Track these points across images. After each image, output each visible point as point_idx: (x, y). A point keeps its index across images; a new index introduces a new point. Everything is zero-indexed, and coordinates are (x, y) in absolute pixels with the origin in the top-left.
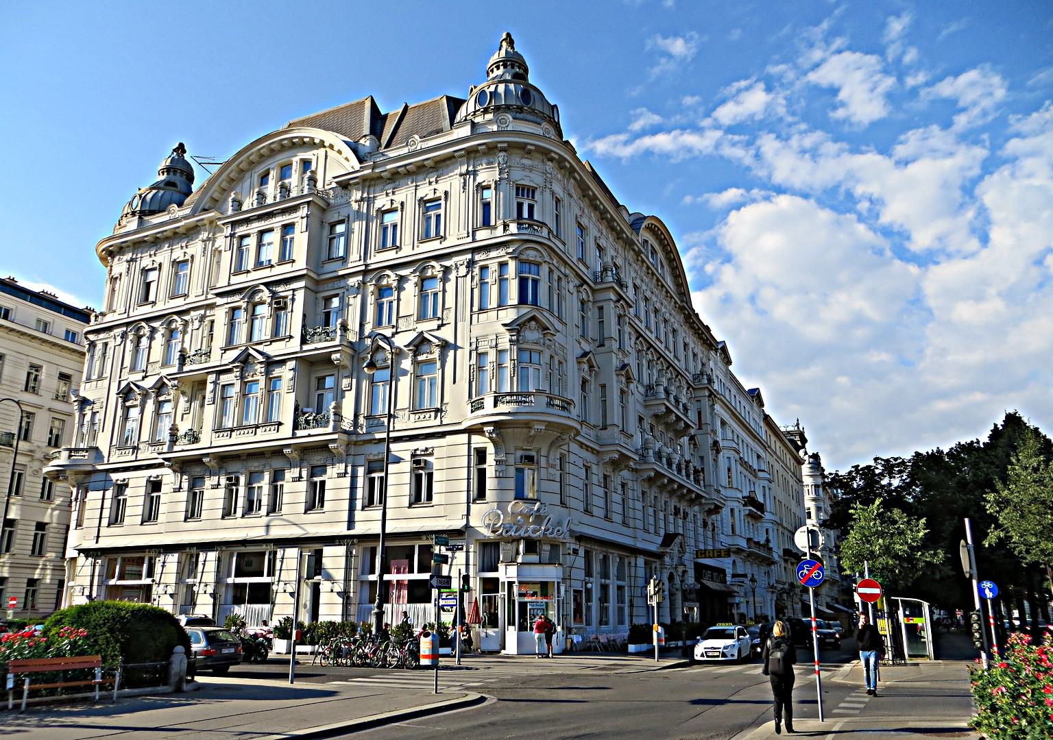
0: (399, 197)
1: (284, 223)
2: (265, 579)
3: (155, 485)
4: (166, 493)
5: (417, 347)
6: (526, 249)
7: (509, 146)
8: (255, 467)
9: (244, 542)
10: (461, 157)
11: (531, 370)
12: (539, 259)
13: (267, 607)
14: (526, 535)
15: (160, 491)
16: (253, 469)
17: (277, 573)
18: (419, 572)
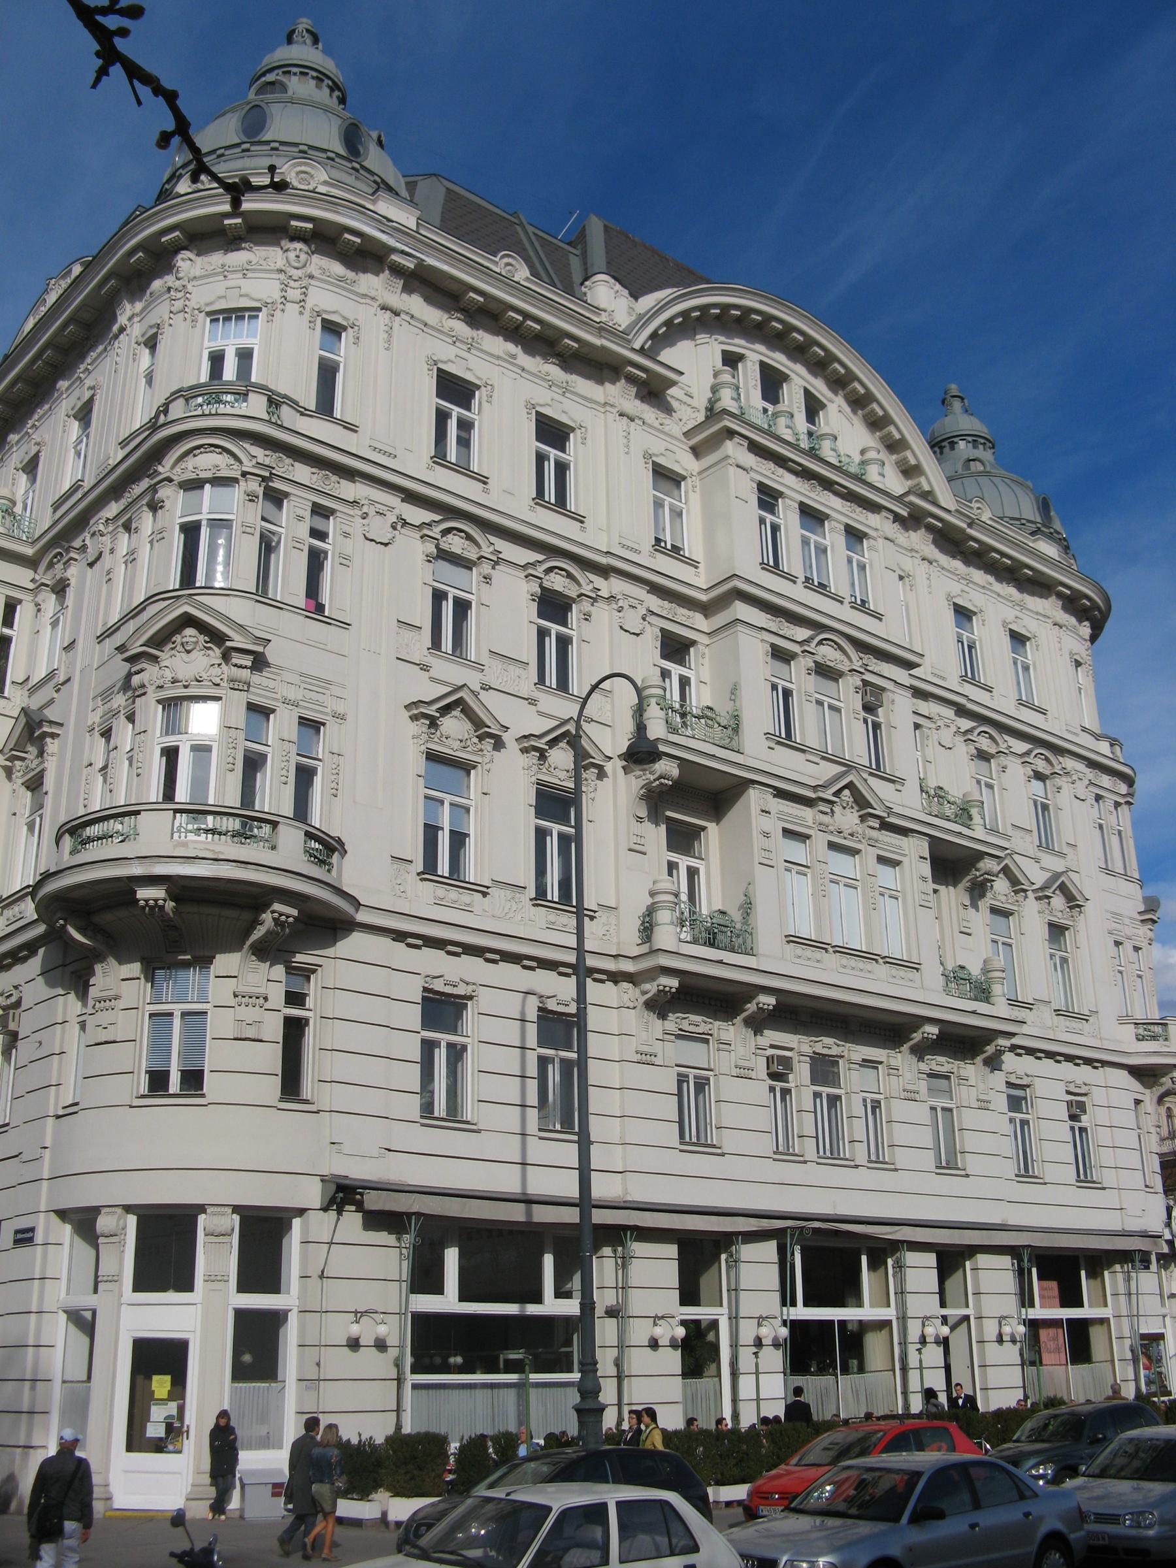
10: (631, 379)
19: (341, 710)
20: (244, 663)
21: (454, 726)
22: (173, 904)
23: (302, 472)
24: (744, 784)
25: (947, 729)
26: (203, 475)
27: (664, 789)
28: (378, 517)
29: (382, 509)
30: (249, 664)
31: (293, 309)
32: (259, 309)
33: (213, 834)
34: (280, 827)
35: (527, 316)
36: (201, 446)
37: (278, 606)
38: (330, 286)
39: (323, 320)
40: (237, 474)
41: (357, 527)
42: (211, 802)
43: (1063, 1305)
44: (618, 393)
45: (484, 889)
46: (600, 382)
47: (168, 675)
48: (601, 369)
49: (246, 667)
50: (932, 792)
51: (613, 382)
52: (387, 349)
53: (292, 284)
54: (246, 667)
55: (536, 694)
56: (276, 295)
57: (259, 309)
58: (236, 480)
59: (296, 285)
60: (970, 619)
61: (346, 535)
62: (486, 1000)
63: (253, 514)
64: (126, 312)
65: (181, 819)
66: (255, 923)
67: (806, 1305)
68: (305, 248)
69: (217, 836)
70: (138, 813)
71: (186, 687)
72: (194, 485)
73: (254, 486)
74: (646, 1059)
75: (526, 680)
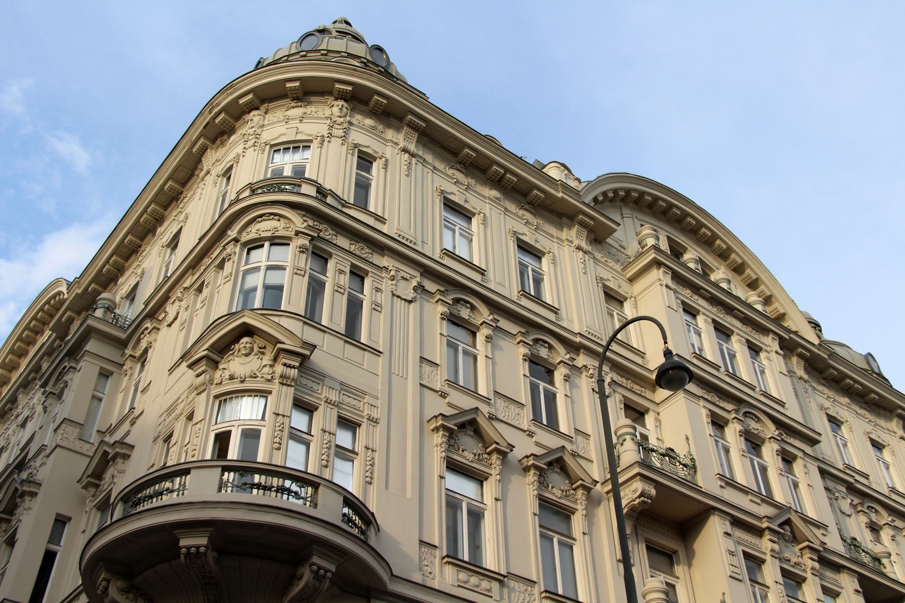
10: (582, 224)
19: (375, 415)
21: (467, 441)
22: (215, 554)
23: (343, 242)
24: (708, 511)
25: (843, 500)
26: (264, 235)
27: (646, 507)
28: (403, 282)
29: (406, 275)
30: (297, 364)
31: (336, 142)
32: (311, 141)
33: (258, 489)
34: (321, 489)
35: (507, 170)
36: (263, 215)
37: (324, 330)
38: (364, 132)
39: (360, 151)
40: (291, 234)
41: (387, 285)
42: (260, 459)
44: (574, 235)
45: (502, 578)
46: (560, 227)
47: (227, 374)
48: (561, 218)
49: (294, 367)
50: (849, 541)
51: (570, 228)
52: (407, 175)
53: (336, 126)
54: (294, 367)
55: (533, 428)
56: (325, 133)
57: (311, 141)
58: (290, 239)
59: (339, 127)
60: (839, 426)
61: (378, 290)
63: (305, 262)
64: (208, 160)
65: (230, 476)
66: (294, 578)
68: (345, 105)
69: (261, 492)
70: (187, 472)
71: (242, 382)
72: (254, 245)
73: (305, 241)
75: (525, 419)
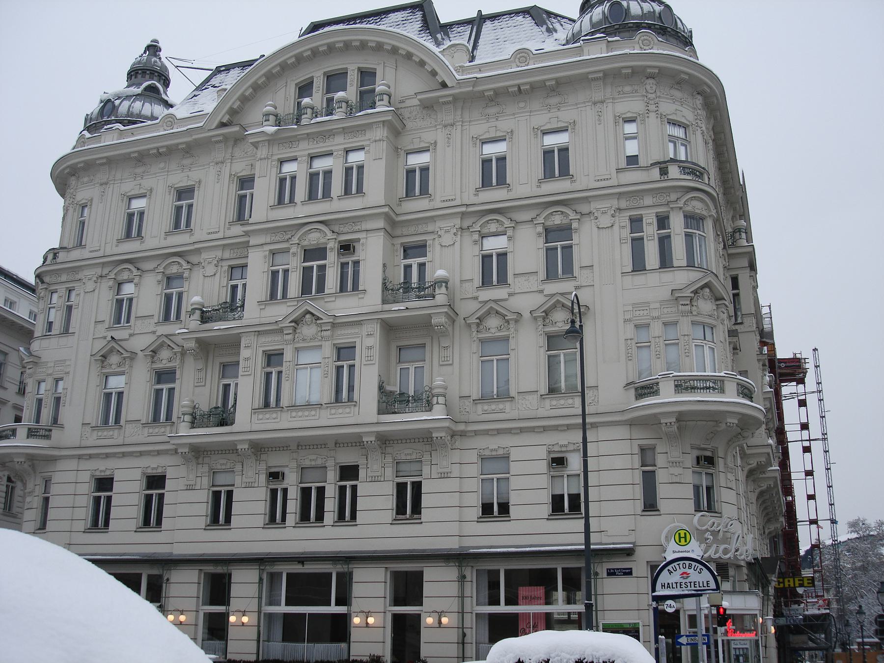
0: (147, 183)
1: (346, 146)
2: (334, 609)
3: (156, 481)
4: (172, 492)
5: (104, 357)
6: (487, 222)
7: (633, 73)
8: (221, 465)
9: (301, 559)
11: (706, 349)
12: (705, 213)
13: (344, 645)
14: (717, 556)
15: (164, 488)
16: (307, 463)
17: (593, 597)
18: (337, 604)
20: (686, 303)
31: (652, 115)
43: (490, 604)
62: (514, 454)
67: (506, 604)
74: (190, 488)
